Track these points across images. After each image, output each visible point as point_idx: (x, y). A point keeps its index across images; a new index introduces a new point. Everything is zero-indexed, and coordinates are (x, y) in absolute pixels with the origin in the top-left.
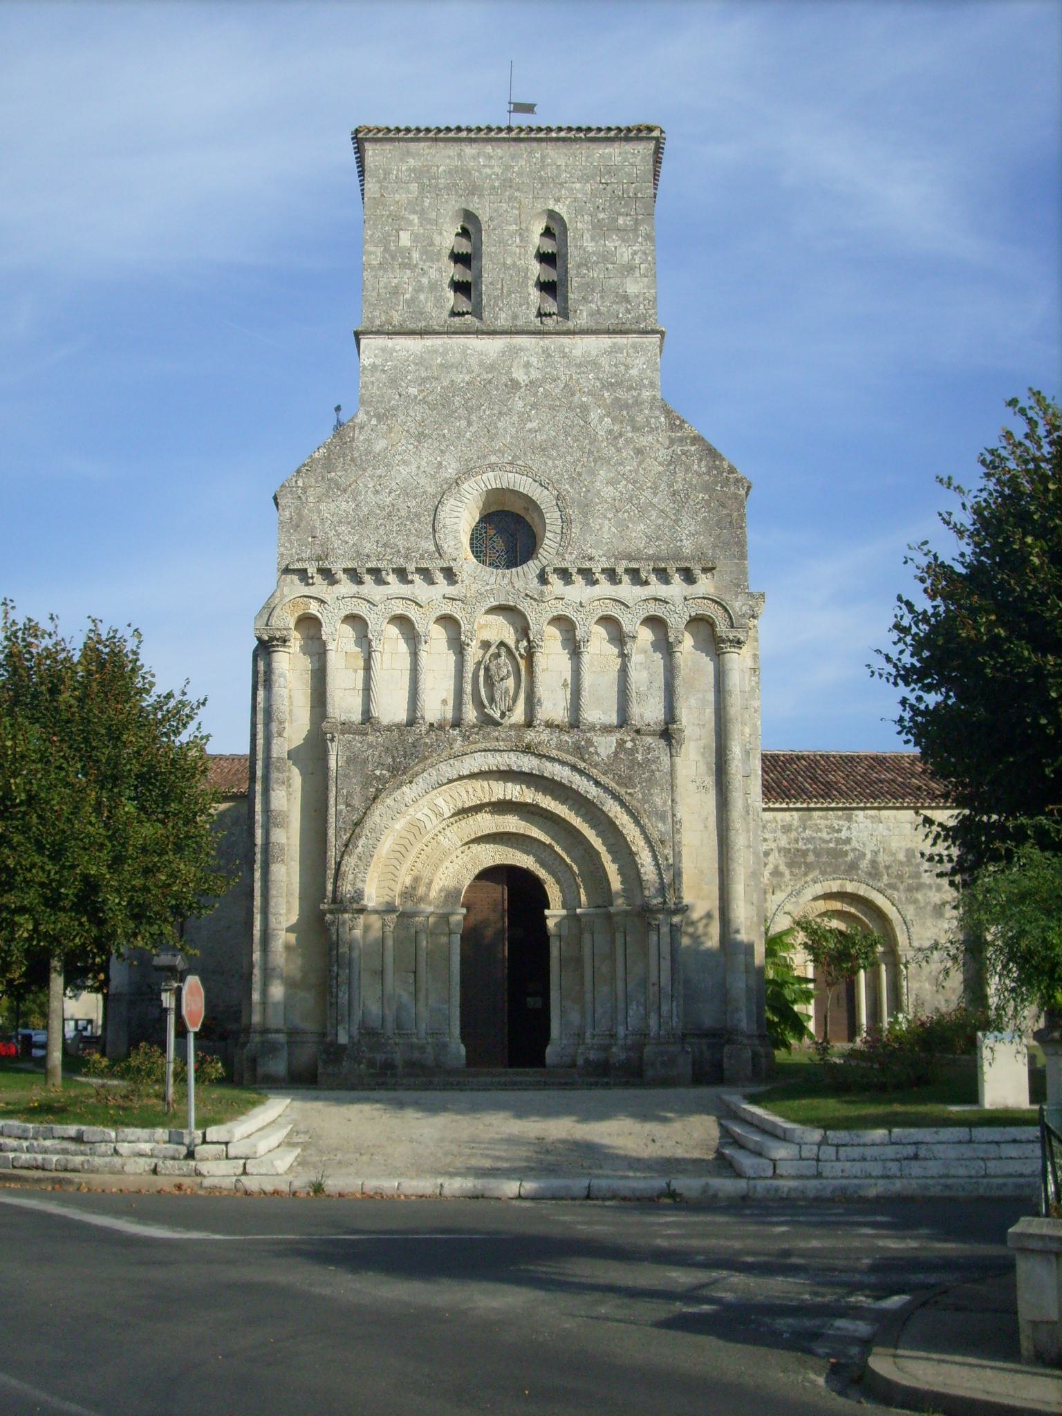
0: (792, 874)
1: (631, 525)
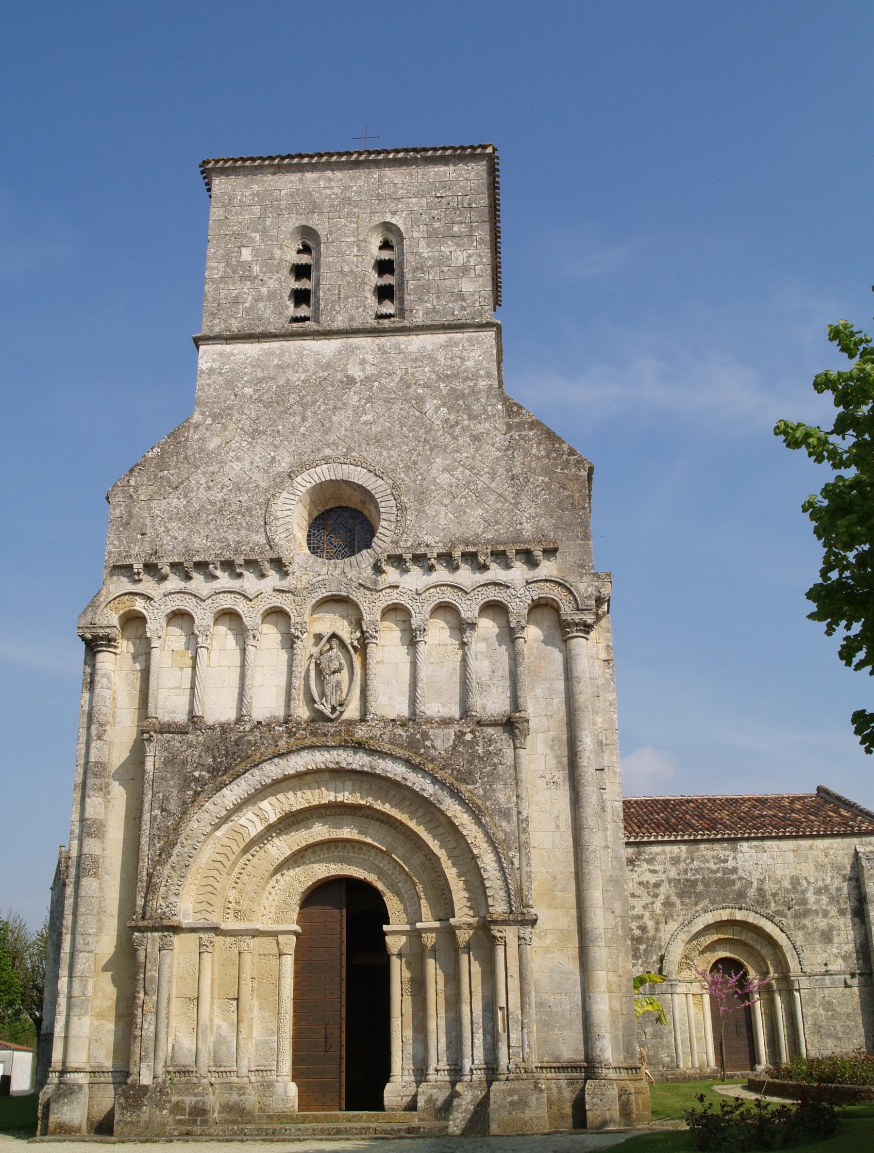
0: (682, 903)
1: (468, 511)
